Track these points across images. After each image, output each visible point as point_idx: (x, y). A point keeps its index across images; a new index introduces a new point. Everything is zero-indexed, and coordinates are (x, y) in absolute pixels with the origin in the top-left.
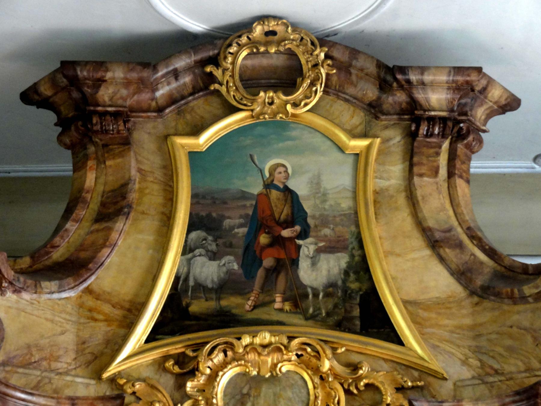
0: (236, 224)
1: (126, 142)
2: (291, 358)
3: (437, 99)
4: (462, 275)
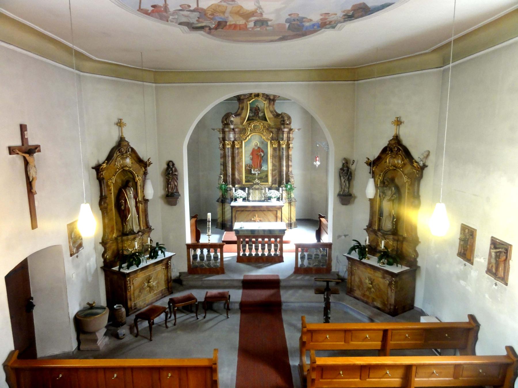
1: (243, 102)
2: (169, 17)
3: (272, 98)
4: (273, 115)
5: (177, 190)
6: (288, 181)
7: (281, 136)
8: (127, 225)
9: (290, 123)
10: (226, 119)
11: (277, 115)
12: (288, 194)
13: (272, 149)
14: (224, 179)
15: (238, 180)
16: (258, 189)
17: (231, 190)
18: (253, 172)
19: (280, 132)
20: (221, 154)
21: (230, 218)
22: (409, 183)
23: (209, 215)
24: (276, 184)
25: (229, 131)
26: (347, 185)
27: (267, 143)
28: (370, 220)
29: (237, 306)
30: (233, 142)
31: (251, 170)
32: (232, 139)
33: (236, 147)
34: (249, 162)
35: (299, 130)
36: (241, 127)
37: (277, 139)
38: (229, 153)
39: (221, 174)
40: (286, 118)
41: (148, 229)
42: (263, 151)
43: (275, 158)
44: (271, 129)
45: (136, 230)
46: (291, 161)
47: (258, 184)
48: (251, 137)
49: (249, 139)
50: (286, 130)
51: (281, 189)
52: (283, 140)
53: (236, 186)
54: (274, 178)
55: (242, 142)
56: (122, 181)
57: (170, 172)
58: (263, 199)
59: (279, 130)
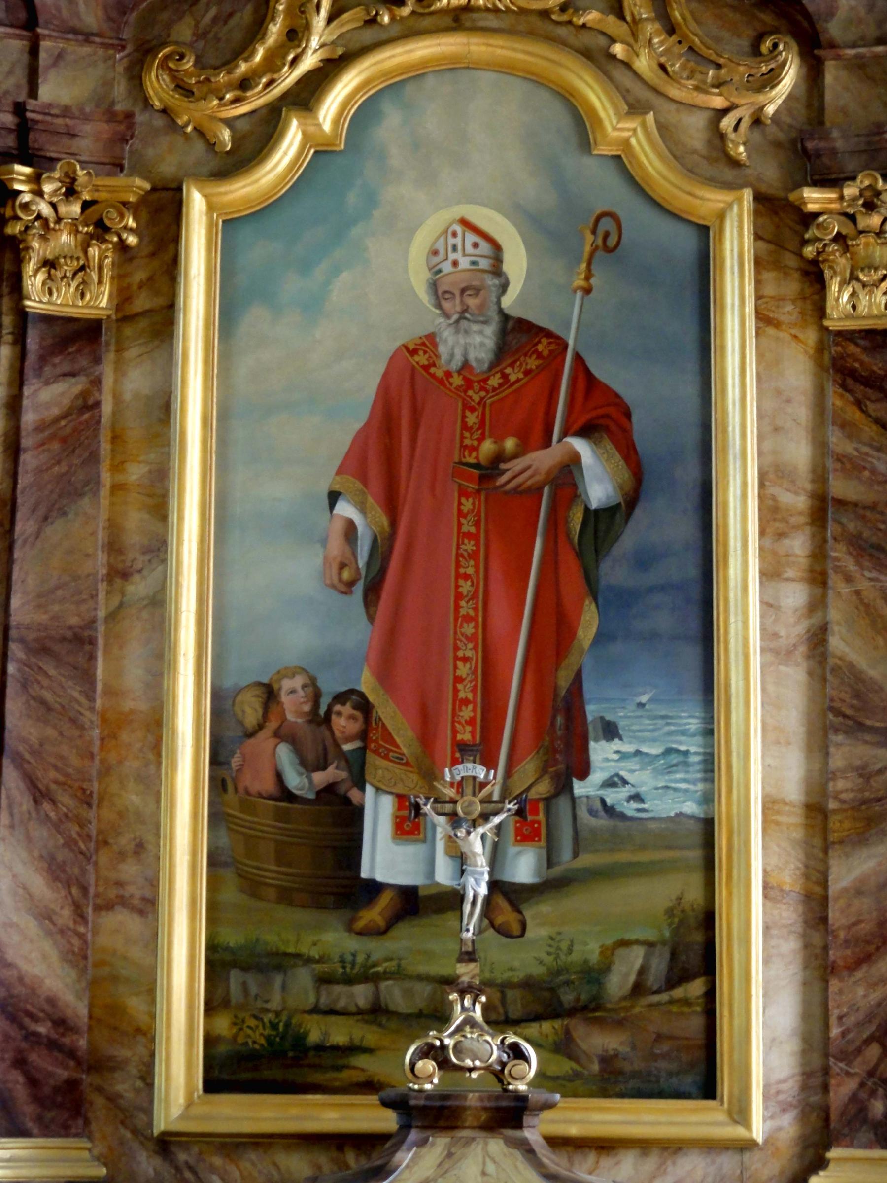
13: (798, 373)
18: (386, 859)
27: (704, 235)
31: (354, 817)
34: (314, 630)
42: (604, 416)
49: (321, 154)
55: (164, 213)
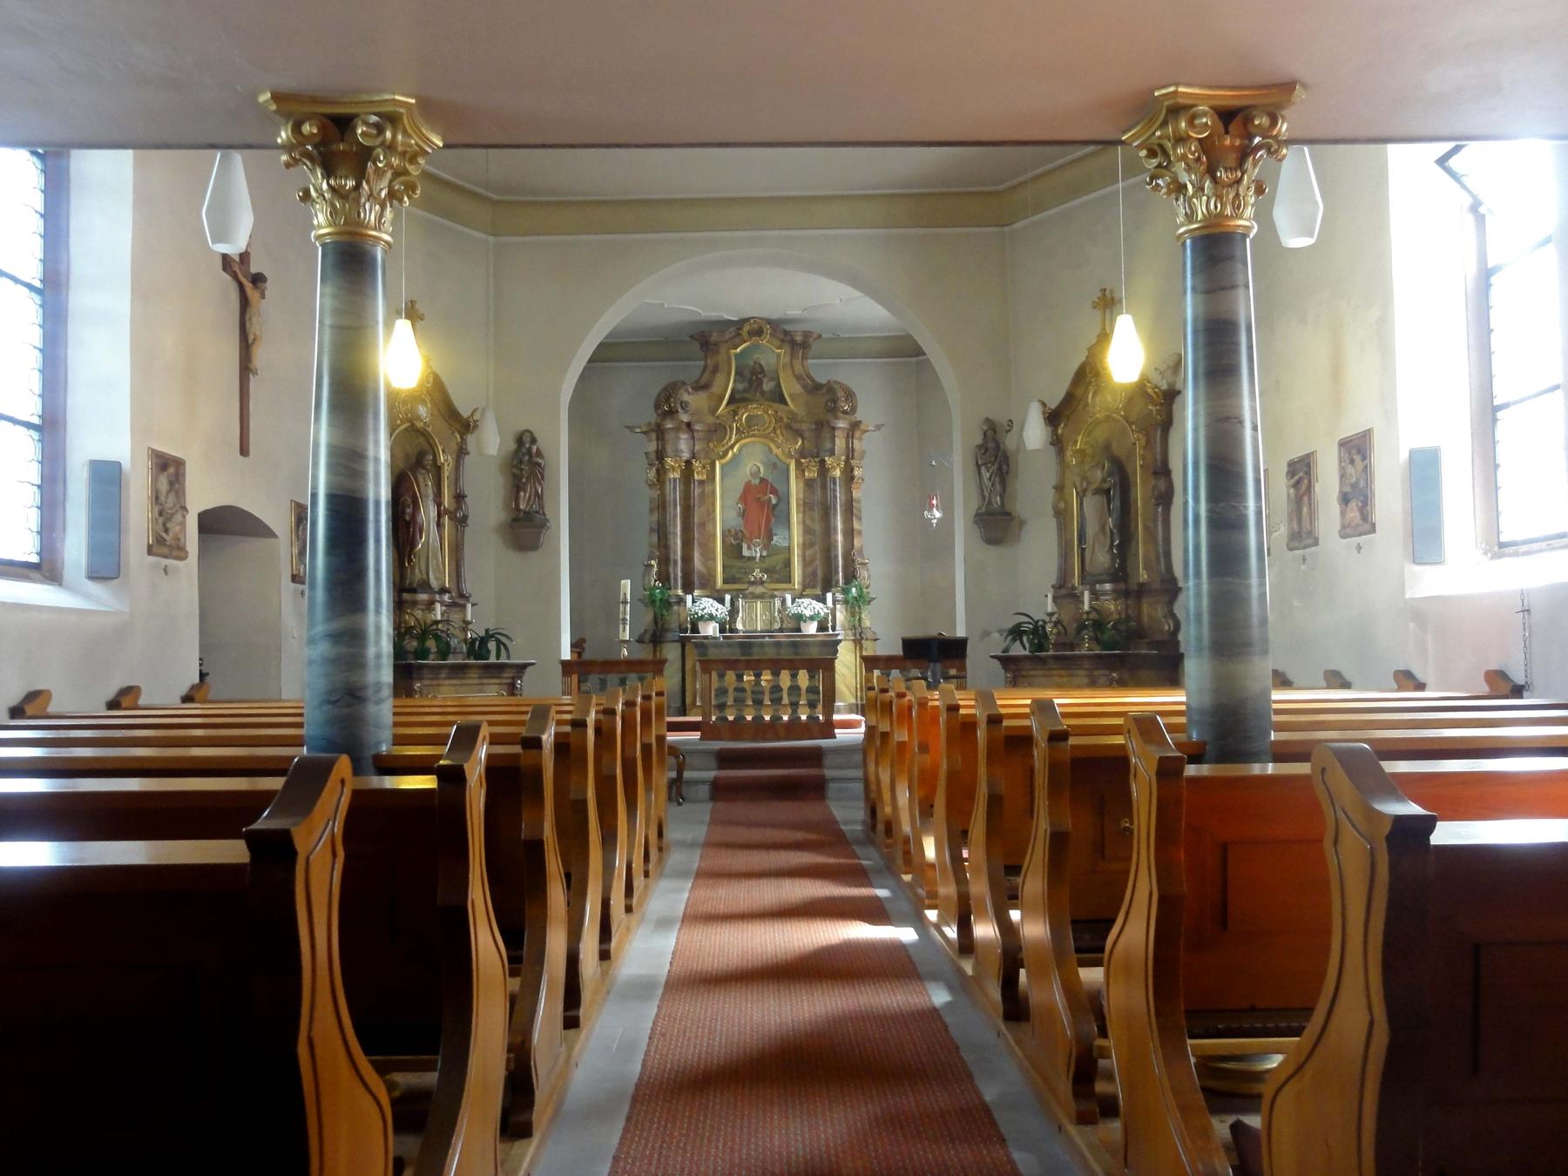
0: (747, 374)
1: (718, 352)
3: (799, 338)
5: (541, 506)
6: (851, 577)
7: (828, 445)
8: (413, 568)
9: (853, 410)
10: (667, 400)
11: (815, 388)
12: (853, 615)
13: (801, 485)
14: (658, 573)
15: (702, 576)
16: (761, 597)
17: (681, 601)
18: (746, 553)
19: (826, 434)
20: (651, 501)
21: (677, 688)
22: (1143, 442)
23: (626, 585)
24: (814, 587)
25: (677, 429)
26: (998, 487)
28: (1060, 569)
29: (704, 791)
30: (688, 463)
32: (686, 456)
33: (696, 477)
35: (878, 427)
36: (710, 420)
37: (815, 453)
38: (675, 494)
39: (651, 558)
40: (840, 394)
41: (460, 600)
42: (774, 491)
43: (812, 509)
44: (796, 426)
45: (434, 583)
46: (859, 519)
47: (762, 583)
48: (740, 450)
50: (842, 424)
51: (829, 596)
52: (832, 453)
53: (696, 593)
54: (810, 569)
56: (407, 457)
57: (525, 463)
58: (777, 626)
59: (823, 428)
